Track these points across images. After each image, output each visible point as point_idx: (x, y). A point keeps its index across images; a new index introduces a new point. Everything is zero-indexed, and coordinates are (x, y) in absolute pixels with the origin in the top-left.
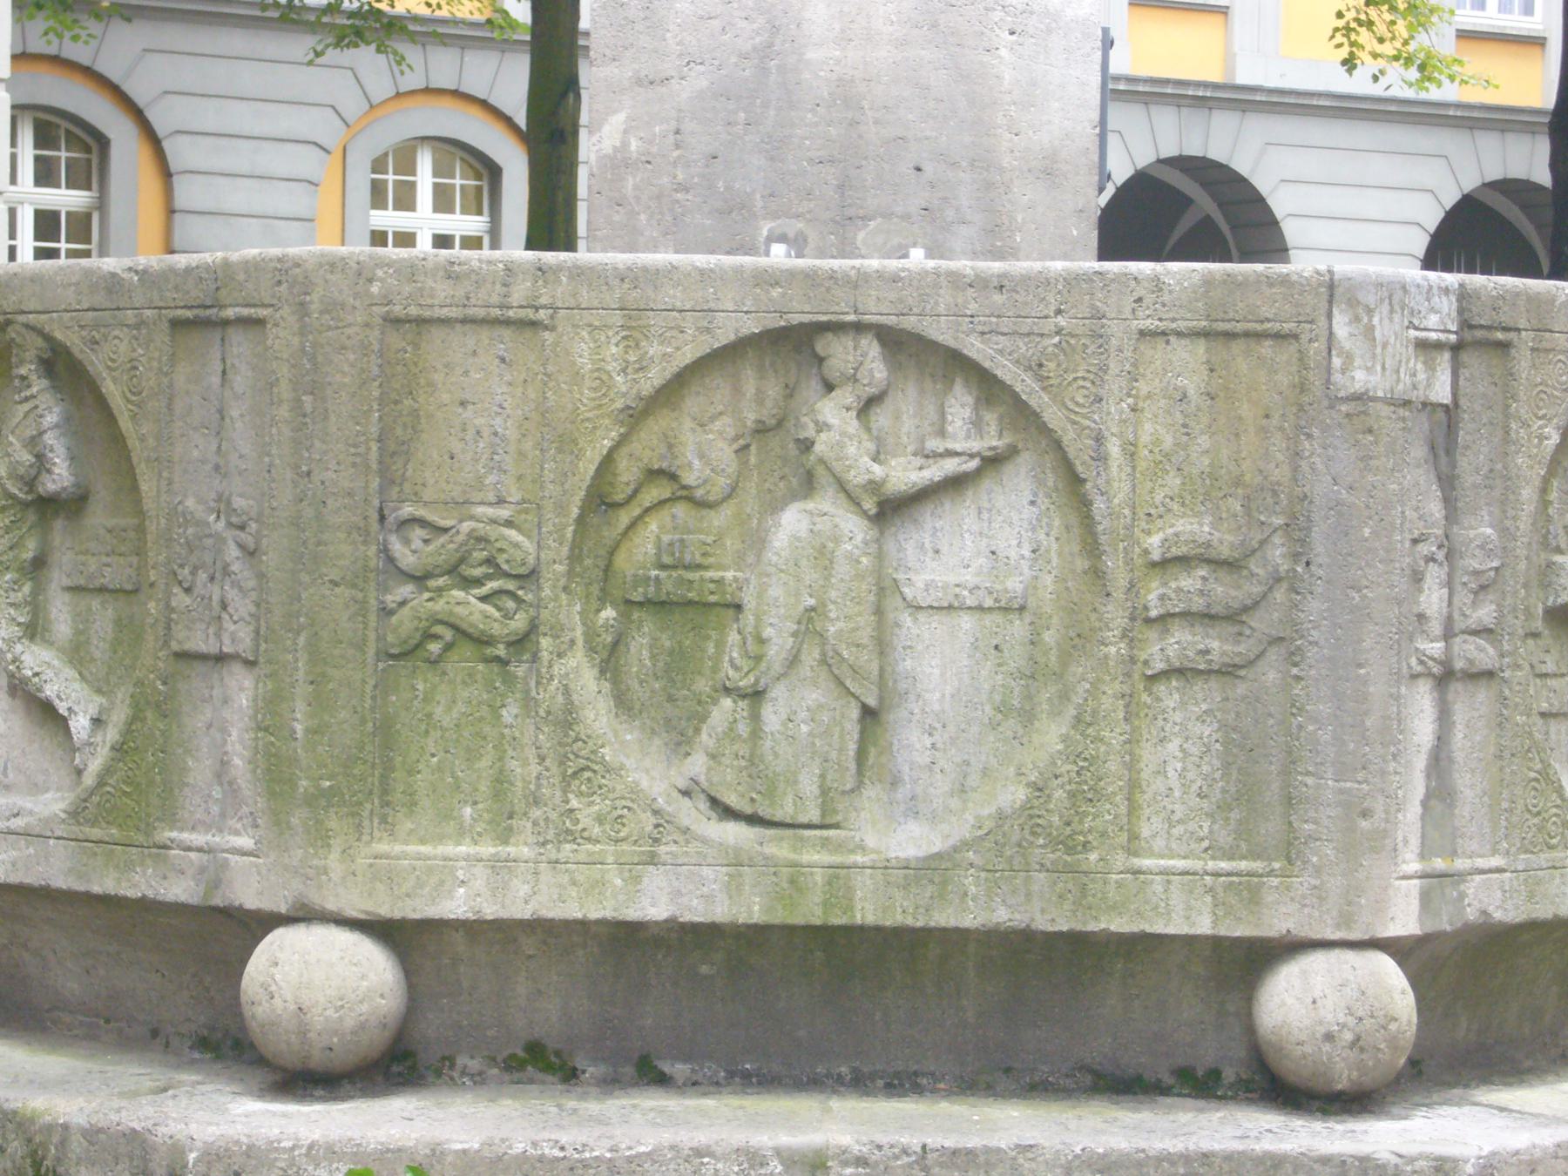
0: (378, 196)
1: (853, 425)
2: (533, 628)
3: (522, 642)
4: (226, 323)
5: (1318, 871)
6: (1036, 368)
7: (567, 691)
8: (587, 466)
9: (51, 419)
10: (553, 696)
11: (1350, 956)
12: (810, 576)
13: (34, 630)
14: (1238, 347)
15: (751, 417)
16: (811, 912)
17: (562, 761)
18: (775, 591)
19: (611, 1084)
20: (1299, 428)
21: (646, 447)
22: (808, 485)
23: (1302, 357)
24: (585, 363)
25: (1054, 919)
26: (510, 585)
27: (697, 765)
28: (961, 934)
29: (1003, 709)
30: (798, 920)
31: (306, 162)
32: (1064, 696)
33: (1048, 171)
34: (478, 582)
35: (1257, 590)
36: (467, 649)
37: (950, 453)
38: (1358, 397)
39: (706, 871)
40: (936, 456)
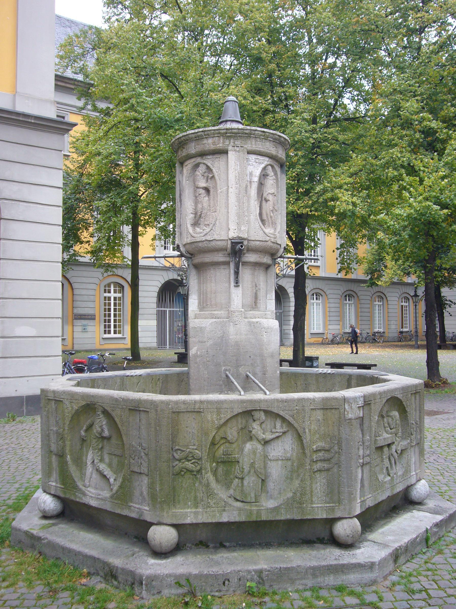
0: (105, 292)
1: (259, 428)
2: (201, 468)
3: (199, 471)
4: (140, 411)
5: (344, 505)
6: (293, 416)
7: (208, 480)
8: (211, 438)
9: (104, 423)
10: (204, 481)
11: (350, 520)
12: (252, 456)
13: (102, 460)
14: (328, 411)
15: (240, 427)
16: (254, 518)
17: (207, 493)
18: (246, 459)
19: (216, 548)
20: (339, 425)
21: (221, 433)
22: (251, 438)
23: (340, 412)
24: (209, 419)
25: (298, 517)
26: (196, 461)
27: (231, 492)
28: (281, 520)
29: (287, 478)
30: (251, 520)
31: (94, 286)
32: (299, 475)
33: (272, 356)
34: (191, 460)
35: (333, 455)
36: (189, 473)
37: (277, 432)
38: (349, 419)
39: (234, 512)
40: (274, 433)
